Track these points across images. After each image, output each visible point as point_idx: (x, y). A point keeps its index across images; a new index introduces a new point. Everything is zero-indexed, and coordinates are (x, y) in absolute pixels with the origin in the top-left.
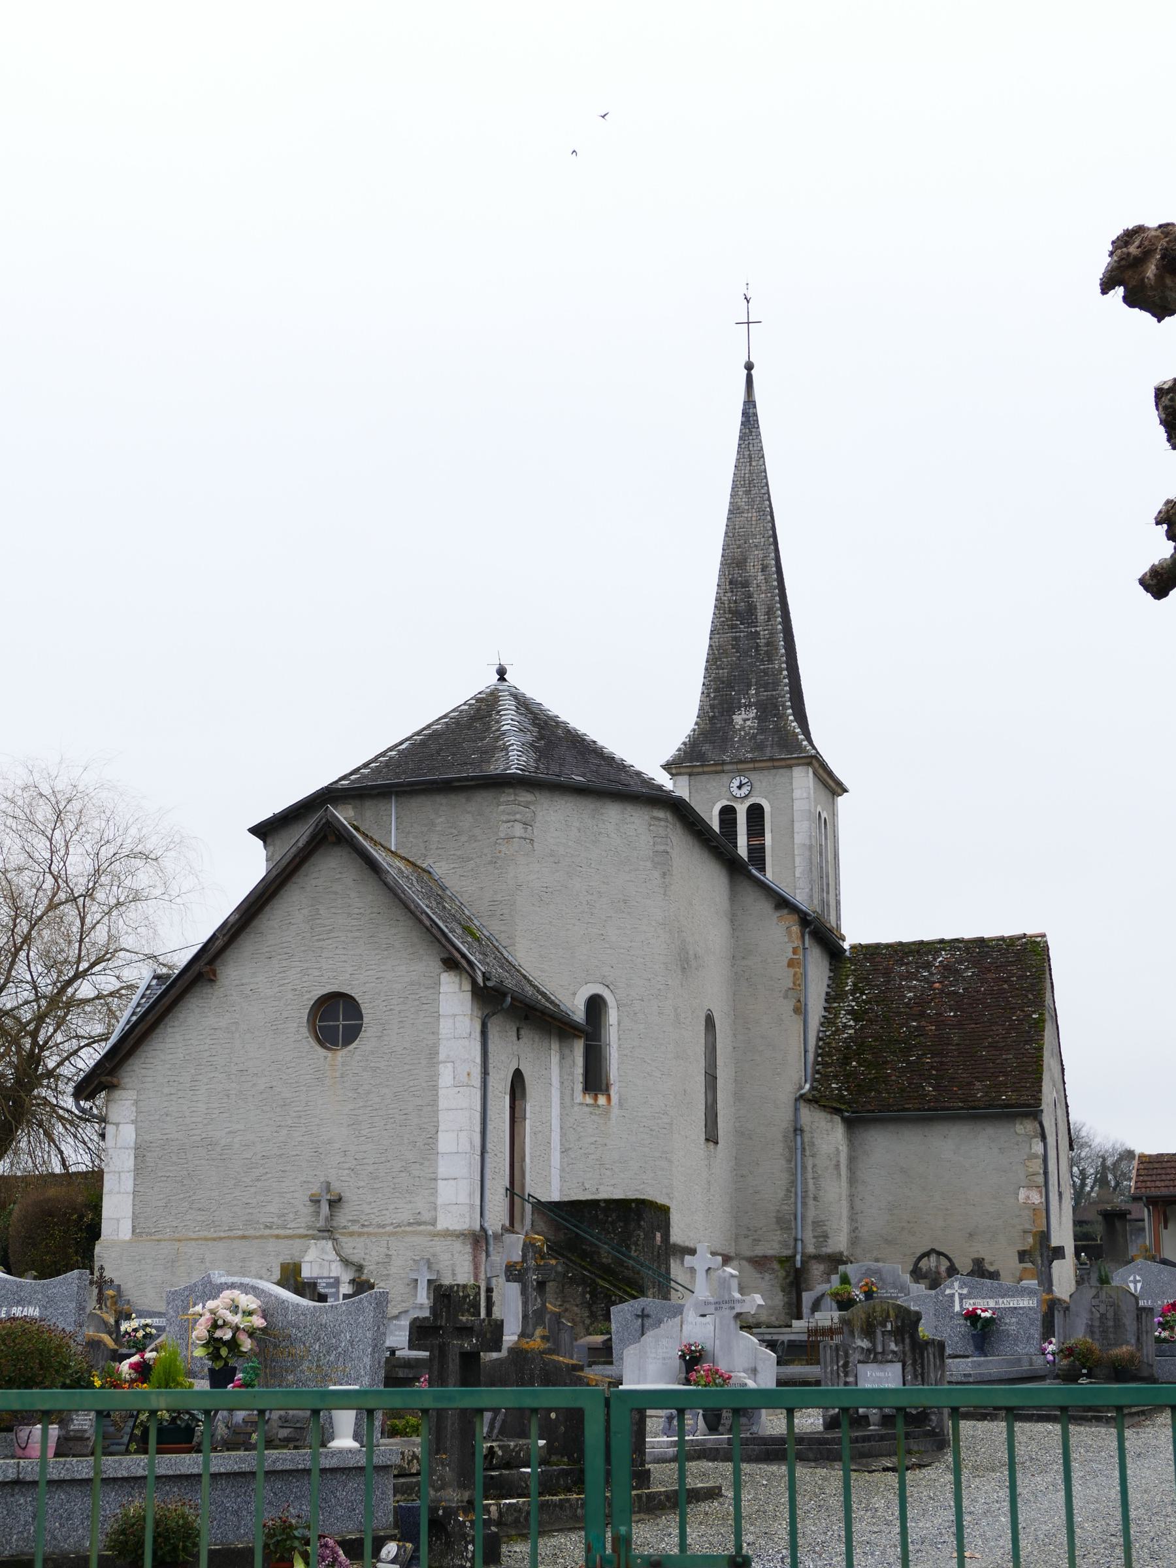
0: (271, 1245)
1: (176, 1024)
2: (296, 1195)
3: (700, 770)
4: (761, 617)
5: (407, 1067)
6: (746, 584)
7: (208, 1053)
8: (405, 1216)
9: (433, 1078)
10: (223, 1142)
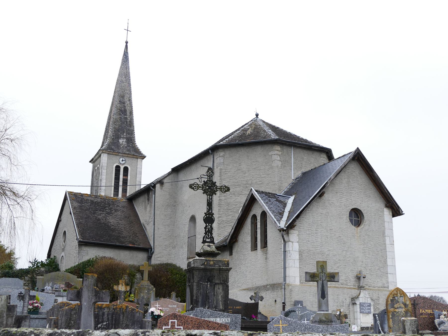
0: (345, 291)
1: (309, 209)
2: (349, 274)
3: (112, 153)
4: (128, 114)
5: (377, 236)
6: (124, 103)
7: (320, 222)
8: (380, 285)
9: (384, 241)
10: (327, 253)
